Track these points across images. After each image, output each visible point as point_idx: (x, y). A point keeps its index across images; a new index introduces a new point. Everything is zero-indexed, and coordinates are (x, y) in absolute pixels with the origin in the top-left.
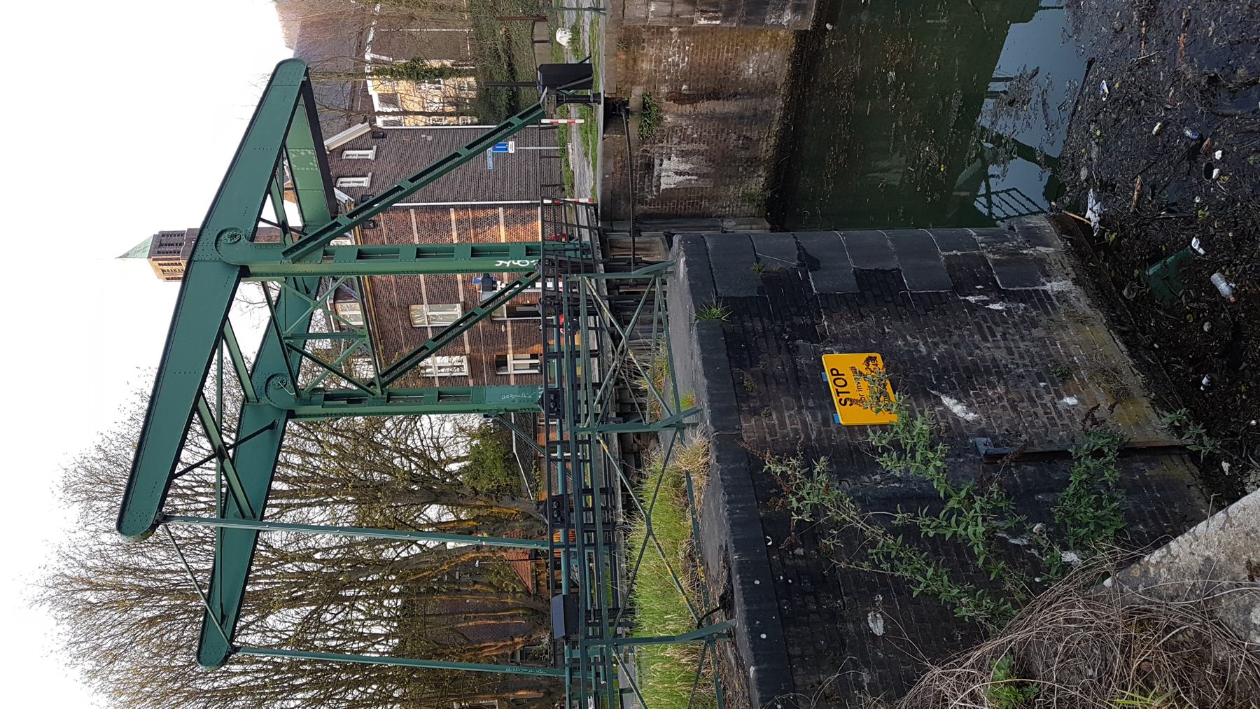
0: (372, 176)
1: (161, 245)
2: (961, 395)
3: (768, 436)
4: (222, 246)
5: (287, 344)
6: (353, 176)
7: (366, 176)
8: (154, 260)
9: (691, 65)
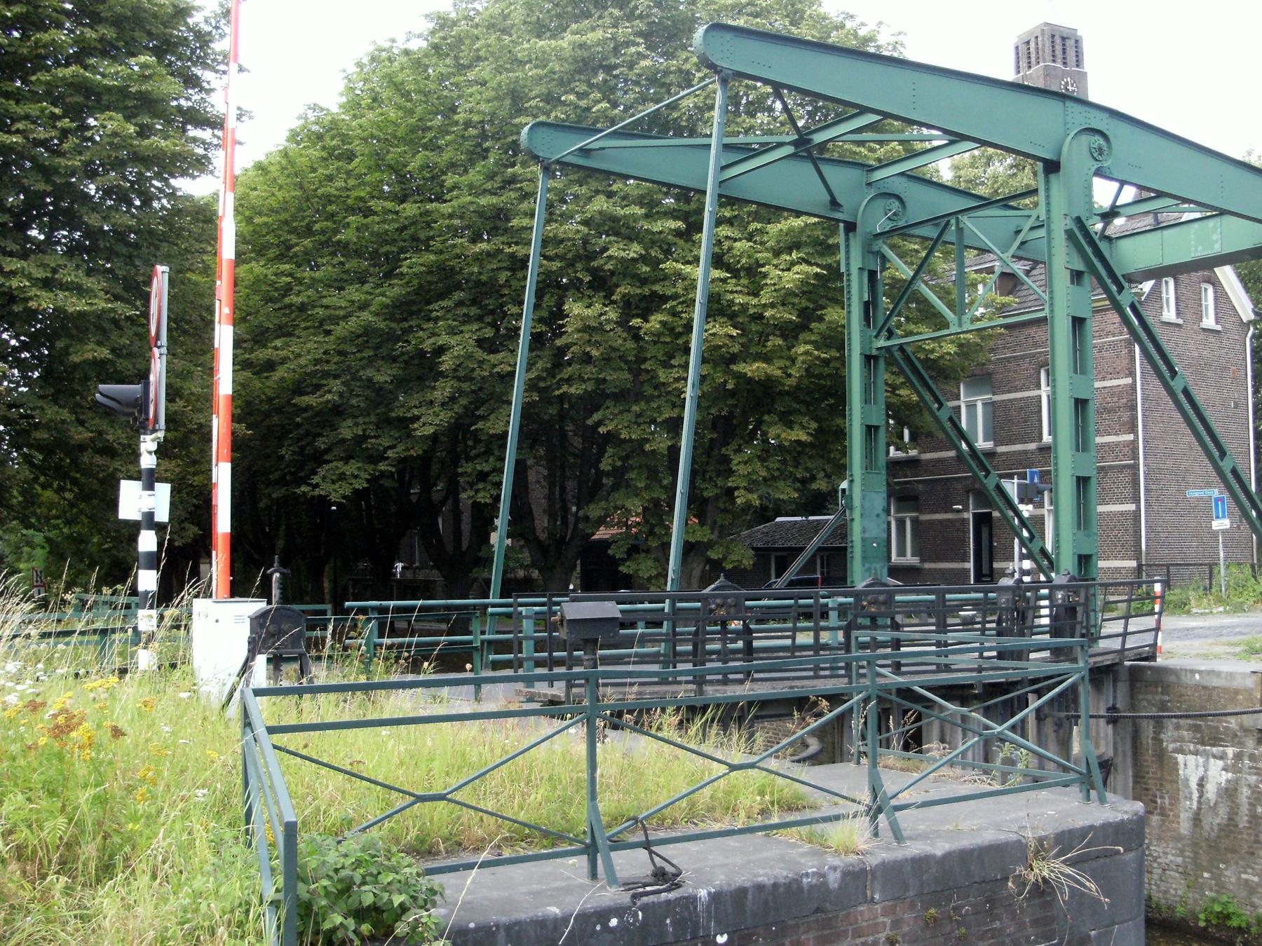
0: (1218, 332)
1: (1063, 39)
4: (1085, 139)
5: (948, 222)
6: (1177, 298)
7: (1179, 314)
8: (1043, 30)
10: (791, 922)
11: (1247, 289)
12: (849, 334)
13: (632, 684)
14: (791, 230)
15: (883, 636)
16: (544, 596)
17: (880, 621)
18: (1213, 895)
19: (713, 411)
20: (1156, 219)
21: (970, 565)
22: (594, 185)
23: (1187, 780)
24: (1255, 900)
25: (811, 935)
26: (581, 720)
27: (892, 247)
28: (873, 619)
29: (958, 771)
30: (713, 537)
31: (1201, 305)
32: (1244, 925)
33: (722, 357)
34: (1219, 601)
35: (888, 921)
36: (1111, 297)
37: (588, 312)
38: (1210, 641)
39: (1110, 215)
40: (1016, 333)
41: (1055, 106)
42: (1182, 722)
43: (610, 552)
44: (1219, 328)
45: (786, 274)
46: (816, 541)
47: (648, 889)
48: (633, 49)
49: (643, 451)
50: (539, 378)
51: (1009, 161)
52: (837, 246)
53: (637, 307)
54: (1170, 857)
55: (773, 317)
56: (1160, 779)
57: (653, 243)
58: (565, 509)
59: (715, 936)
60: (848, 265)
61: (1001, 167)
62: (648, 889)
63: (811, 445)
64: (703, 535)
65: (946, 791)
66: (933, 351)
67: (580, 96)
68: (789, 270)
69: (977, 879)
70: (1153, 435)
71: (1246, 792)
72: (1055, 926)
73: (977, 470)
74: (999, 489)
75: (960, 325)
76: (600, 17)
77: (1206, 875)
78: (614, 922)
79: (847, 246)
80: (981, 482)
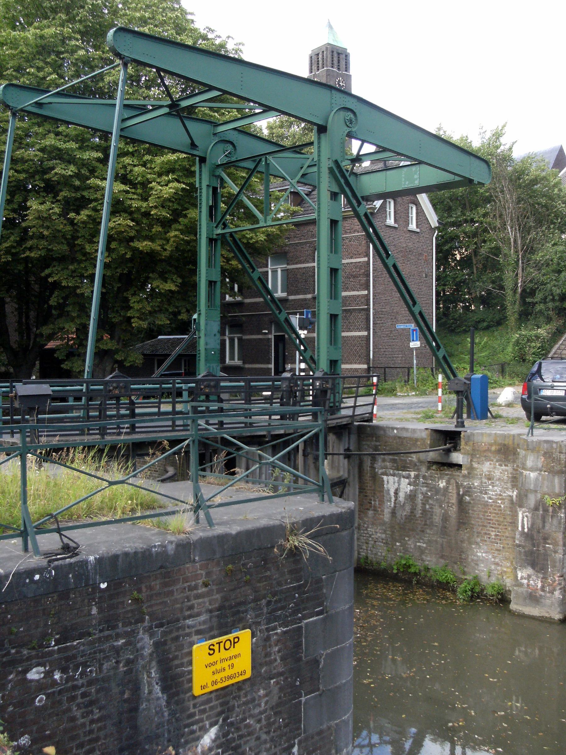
0: (395, 228)
1: (339, 54)
2: (218, 742)
3: (188, 584)
4: (342, 114)
5: (261, 160)
6: (395, 212)
7: (396, 221)
8: (327, 48)
9: (486, 505)
10: (146, 575)
11: (435, 209)
12: (200, 225)
13: (55, 436)
14: (169, 161)
15: (214, 406)
16: (7, 382)
17: (212, 398)
18: (401, 554)
19: (119, 270)
20: (385, 164)
21: (272, 366)
22: (47, 126)
23: (389, 490)
24: (424, 557)
25: (158, 582)
26: (16, 456)
27: (229, 175)
28: (207, 396)
29: (250, 485)
30: (117, 347)
31: (408, 217)
32: (417, 571)
33: (124, 238)
34: (413, 389)
35: (203, 572)
36: (354, 210)
37: (42, 207)
38: (405, 411)
39: (358, 159)
40: (302, 228)
41: (324, 93)
42: (386, 457)
43: (55, 355)
44: (418, 230)
45: (164, 188)
46: (178, 350)
47: (58, 557)
48: (73, 43)
49: (76, 294)
50: (12, 247)
51: (303, 125)
52: (194, 172)
53: (74, 205)
54: (379, 535)
55: (156, 214)
56: (374, 490)
57: (83, 165)
58: (29, 329)
59: (100, 583)
60: (200, 183)
61: (297, 129)
62: (58, 557)
63: (178, 292)
64: (109, 344)
65: (242, 497)
66: (252, 238)
67: (39, 69)
68: (167, 185)
69: (256, 547)
70: (379, 291)
71: (420, 497)
72: (302, 573)
73: (275, 310)
74: (287, 321)
75: (266, 222)
76: (54, 19)
77: (398, 544)
78: (37, 577)
79: (200, 171)
80: (277, 317)
